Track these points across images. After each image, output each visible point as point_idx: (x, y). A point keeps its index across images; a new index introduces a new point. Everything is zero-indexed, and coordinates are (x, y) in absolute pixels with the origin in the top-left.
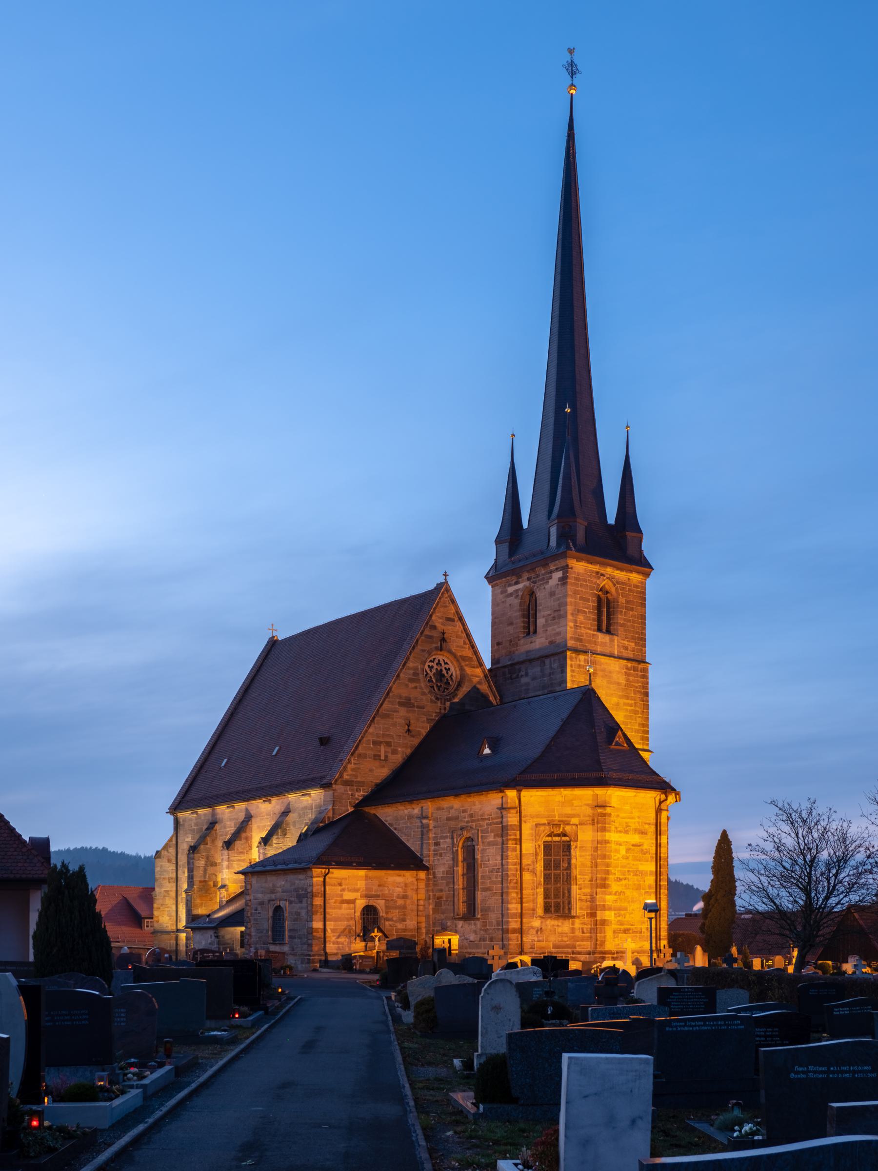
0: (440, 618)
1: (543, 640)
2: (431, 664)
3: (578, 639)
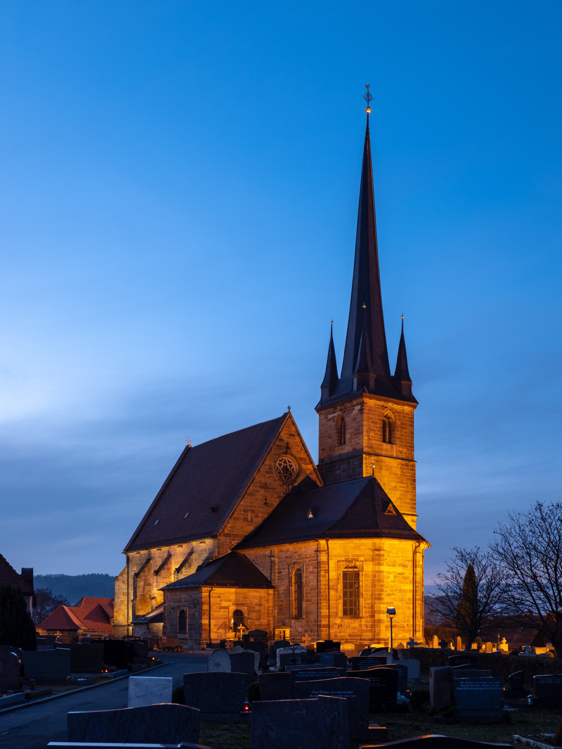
0: (285, 434)
1: (349, 447)
2: (280, 462)
3: (371, 447)
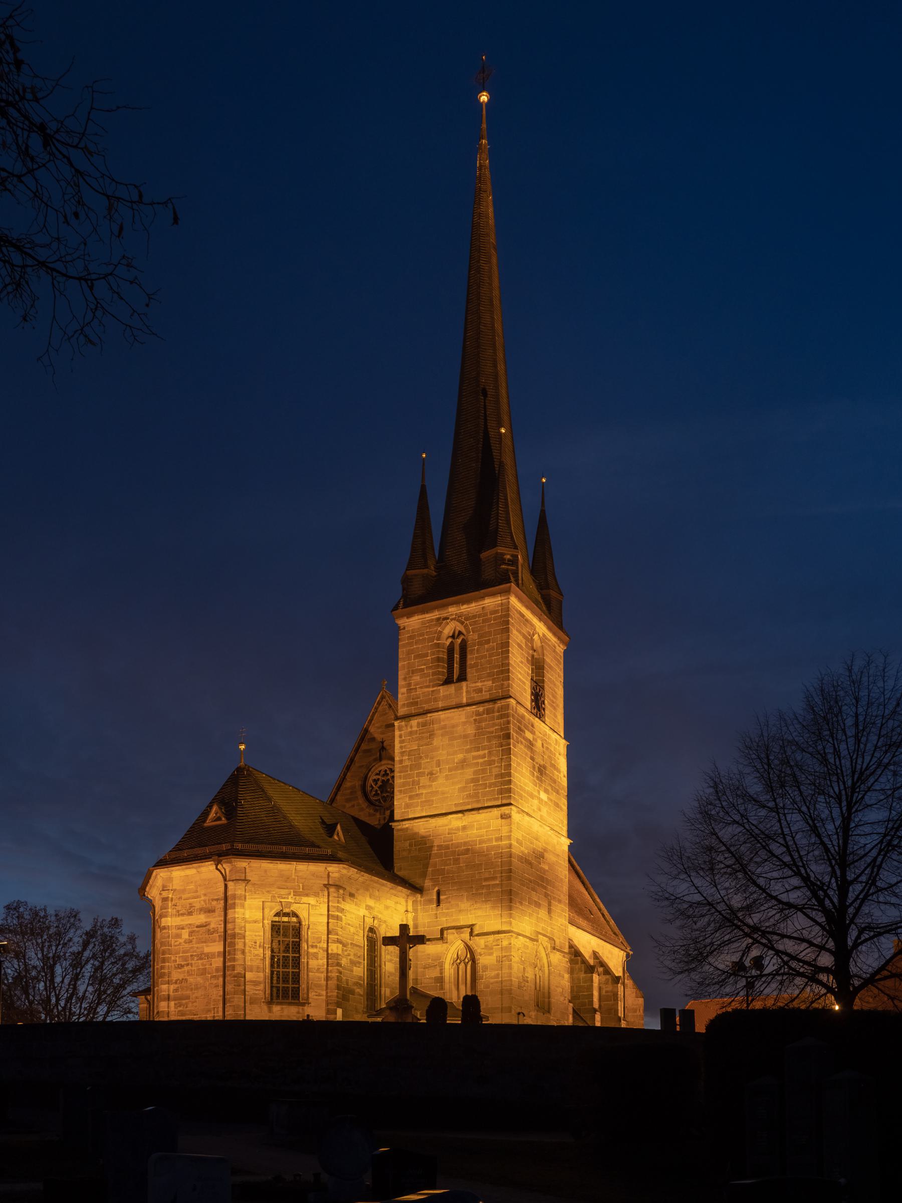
0: (379, 728)
